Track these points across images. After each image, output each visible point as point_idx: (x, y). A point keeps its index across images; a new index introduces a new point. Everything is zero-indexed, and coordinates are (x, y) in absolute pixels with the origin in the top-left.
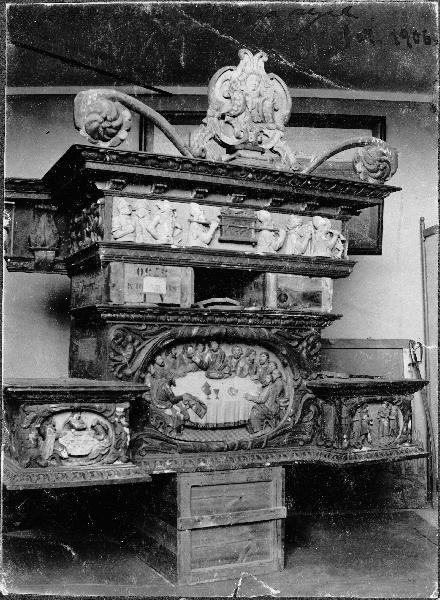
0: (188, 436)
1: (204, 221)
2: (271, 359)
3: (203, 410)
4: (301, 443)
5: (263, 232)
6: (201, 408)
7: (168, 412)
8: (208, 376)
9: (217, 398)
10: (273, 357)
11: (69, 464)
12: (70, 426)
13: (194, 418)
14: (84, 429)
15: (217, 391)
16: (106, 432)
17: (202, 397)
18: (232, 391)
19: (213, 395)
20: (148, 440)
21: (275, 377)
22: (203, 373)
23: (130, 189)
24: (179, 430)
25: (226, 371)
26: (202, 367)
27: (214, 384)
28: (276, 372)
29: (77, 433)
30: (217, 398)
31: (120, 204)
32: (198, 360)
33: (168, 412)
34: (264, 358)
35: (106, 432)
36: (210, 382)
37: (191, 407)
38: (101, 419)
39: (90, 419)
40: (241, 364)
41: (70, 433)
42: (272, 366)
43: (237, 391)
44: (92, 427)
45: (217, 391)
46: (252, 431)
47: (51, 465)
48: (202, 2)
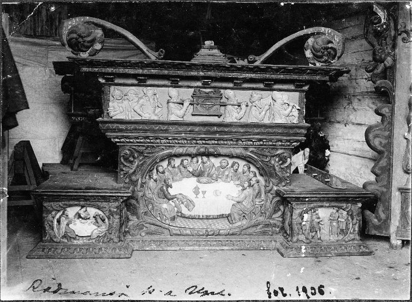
0: (180, 222)
1: (178, 101)
2: (251, 170)
3: (192, 206)
4: (270, 233)
5: (229, 107)
6: (190, 204)
7: (165, 206)
8: (199, 181)
9: (204, 197)
10: (253, 169)
11: (75, 241)
12: (79, 216)
13: (185, 211)
14: (89, 218)
15: (204, 192)
16: (103, 221)
17: (192, 196)
18: (216, 193)
19: (201, 195)
20: (147, 225)
21: (252, 182)
22: (196, 178)
23: (149, 82)
24: (173, 219)
25: (213, 179)
26: (198, 175)
27: (202, 187)
28: (254, 179)
29: (83, 221)
30: (204, 197)
31: (115, 91)
32: (191, 170)
33: (165, 206)
34: (246, 169)
35: (103, 221)
36: (200, 185)
37: (182, 203)
38: (100, 212)
39: (92, 211)
40: (227, 173)
41: (78, 221)
42: (251, 175)
43: (221, 193)
44: (94, 217)
45: (204, 192)
46: (231, 222)
47: (63, 242)
48: (360, 2)
